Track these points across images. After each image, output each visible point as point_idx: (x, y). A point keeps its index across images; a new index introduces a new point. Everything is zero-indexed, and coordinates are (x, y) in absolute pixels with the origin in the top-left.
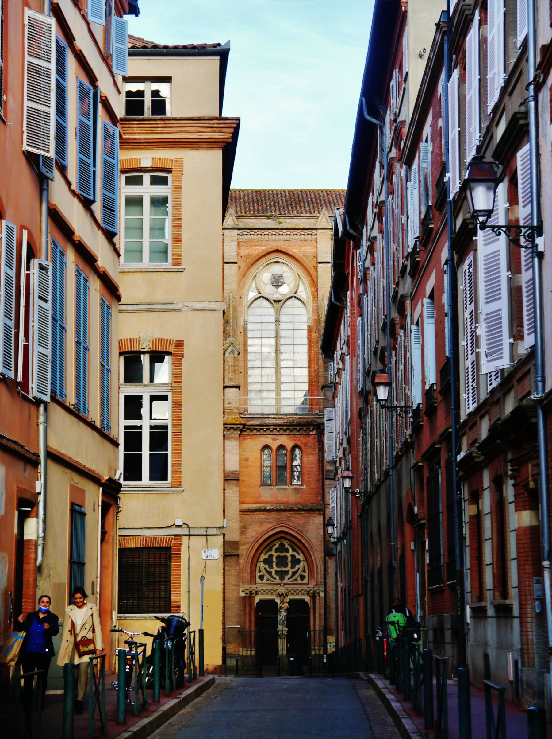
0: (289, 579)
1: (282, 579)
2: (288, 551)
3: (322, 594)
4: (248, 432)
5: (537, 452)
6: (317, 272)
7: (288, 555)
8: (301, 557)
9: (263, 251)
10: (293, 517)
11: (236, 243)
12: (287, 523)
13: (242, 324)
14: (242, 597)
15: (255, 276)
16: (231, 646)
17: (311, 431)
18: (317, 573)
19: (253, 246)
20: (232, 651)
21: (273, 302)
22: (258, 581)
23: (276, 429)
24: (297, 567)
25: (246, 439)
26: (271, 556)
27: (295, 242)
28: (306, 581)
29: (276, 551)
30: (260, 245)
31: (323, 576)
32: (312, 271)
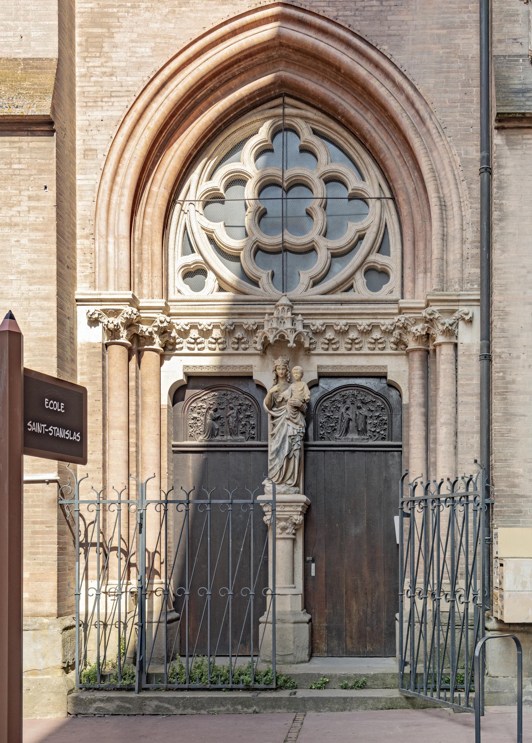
3: (469, 337)
5: (206, 645)
18: (444, 238)
28: (390, 289)
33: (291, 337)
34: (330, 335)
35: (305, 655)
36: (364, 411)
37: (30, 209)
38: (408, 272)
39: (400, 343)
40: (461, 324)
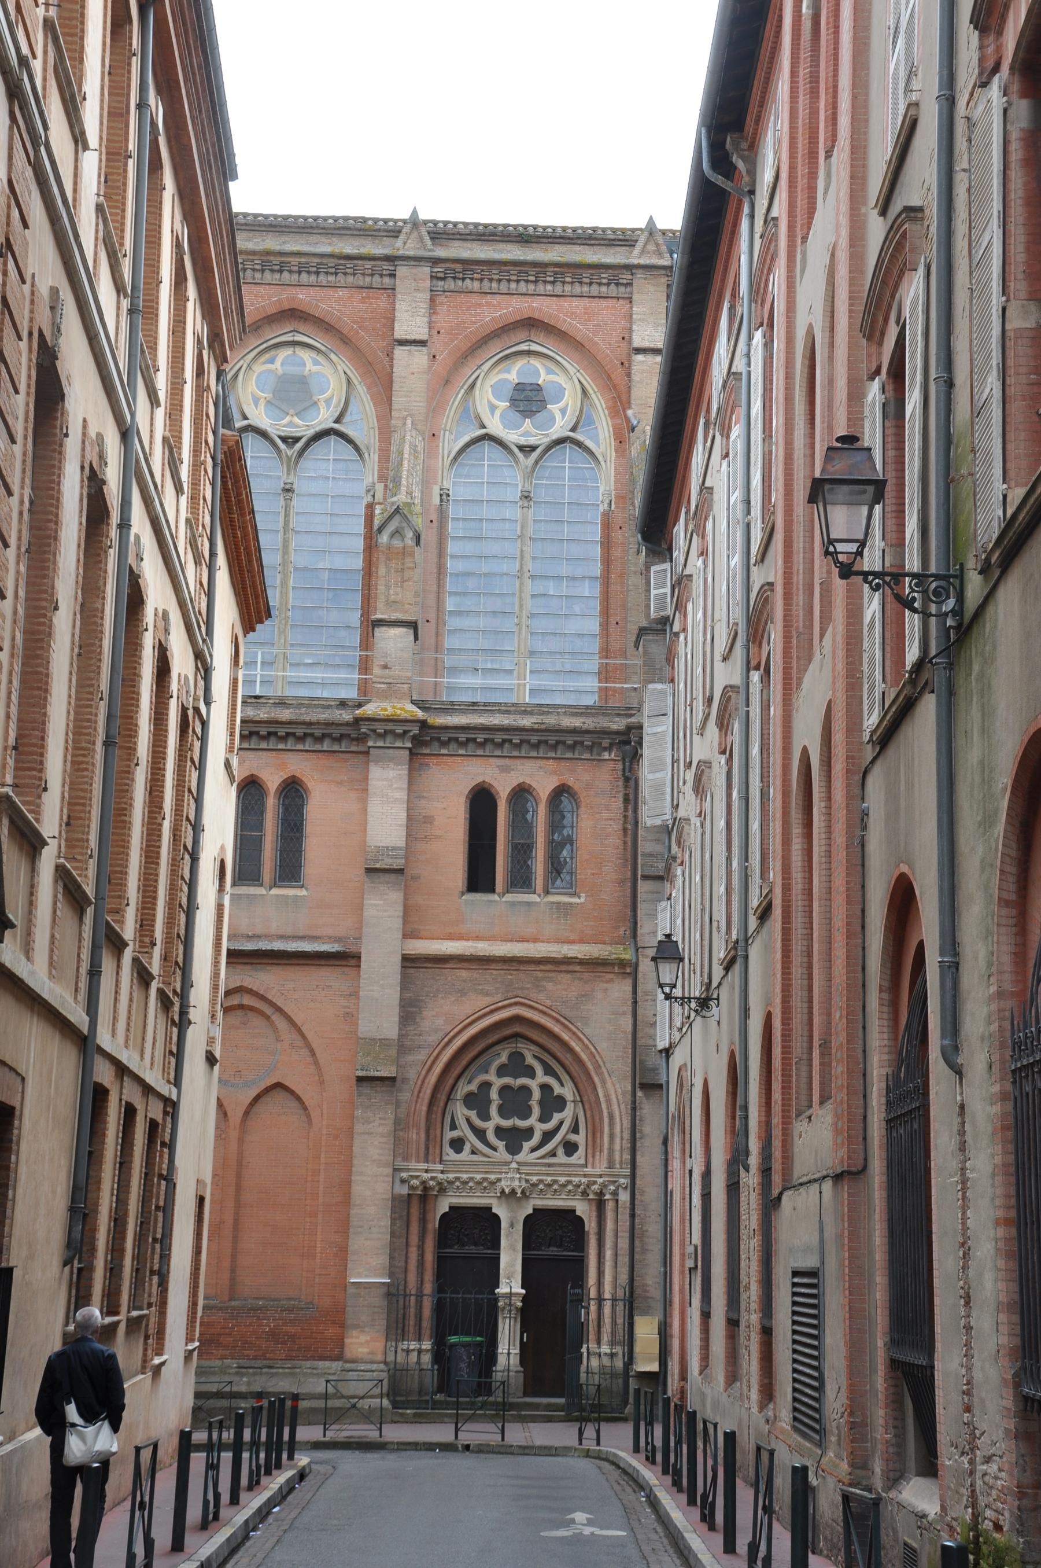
0: (533, 1150)
1: (514, 1149)
2: (531, 1073)
3: (624, 1197)
4: (435, 748)
6: (629, 375)
7: (534, 1085)
8: (567, 1091)
9: (493, 319)
10: (550, 980)
11: (427, 296)
12: (533, 995)
13: (437, 501)
14: (401, 1196)
15: (472, 386)
16: (363, 1338)
17: (605, 749)
18: (612, 1136)
19: (468, 308)
20: (366, 1350)
21: (516, 450)
22: (450, 1154)
23: (510, 741)
24: (557, 1117)
25: (427, 765)
26: (486, 1085)
27: (575, 302)
28: (578, 1157)
29: (501, 1071)
30: (488, 304)
31: (627, 1145)
32: (618, 374)
33: (519, 1191)
34: (541, 1186)
35: (521, 1394)
36: (560, 1232)
37: (380, 1125)
38: (590, 1151)
39: (584, 1193)
40: (620, 1190)
